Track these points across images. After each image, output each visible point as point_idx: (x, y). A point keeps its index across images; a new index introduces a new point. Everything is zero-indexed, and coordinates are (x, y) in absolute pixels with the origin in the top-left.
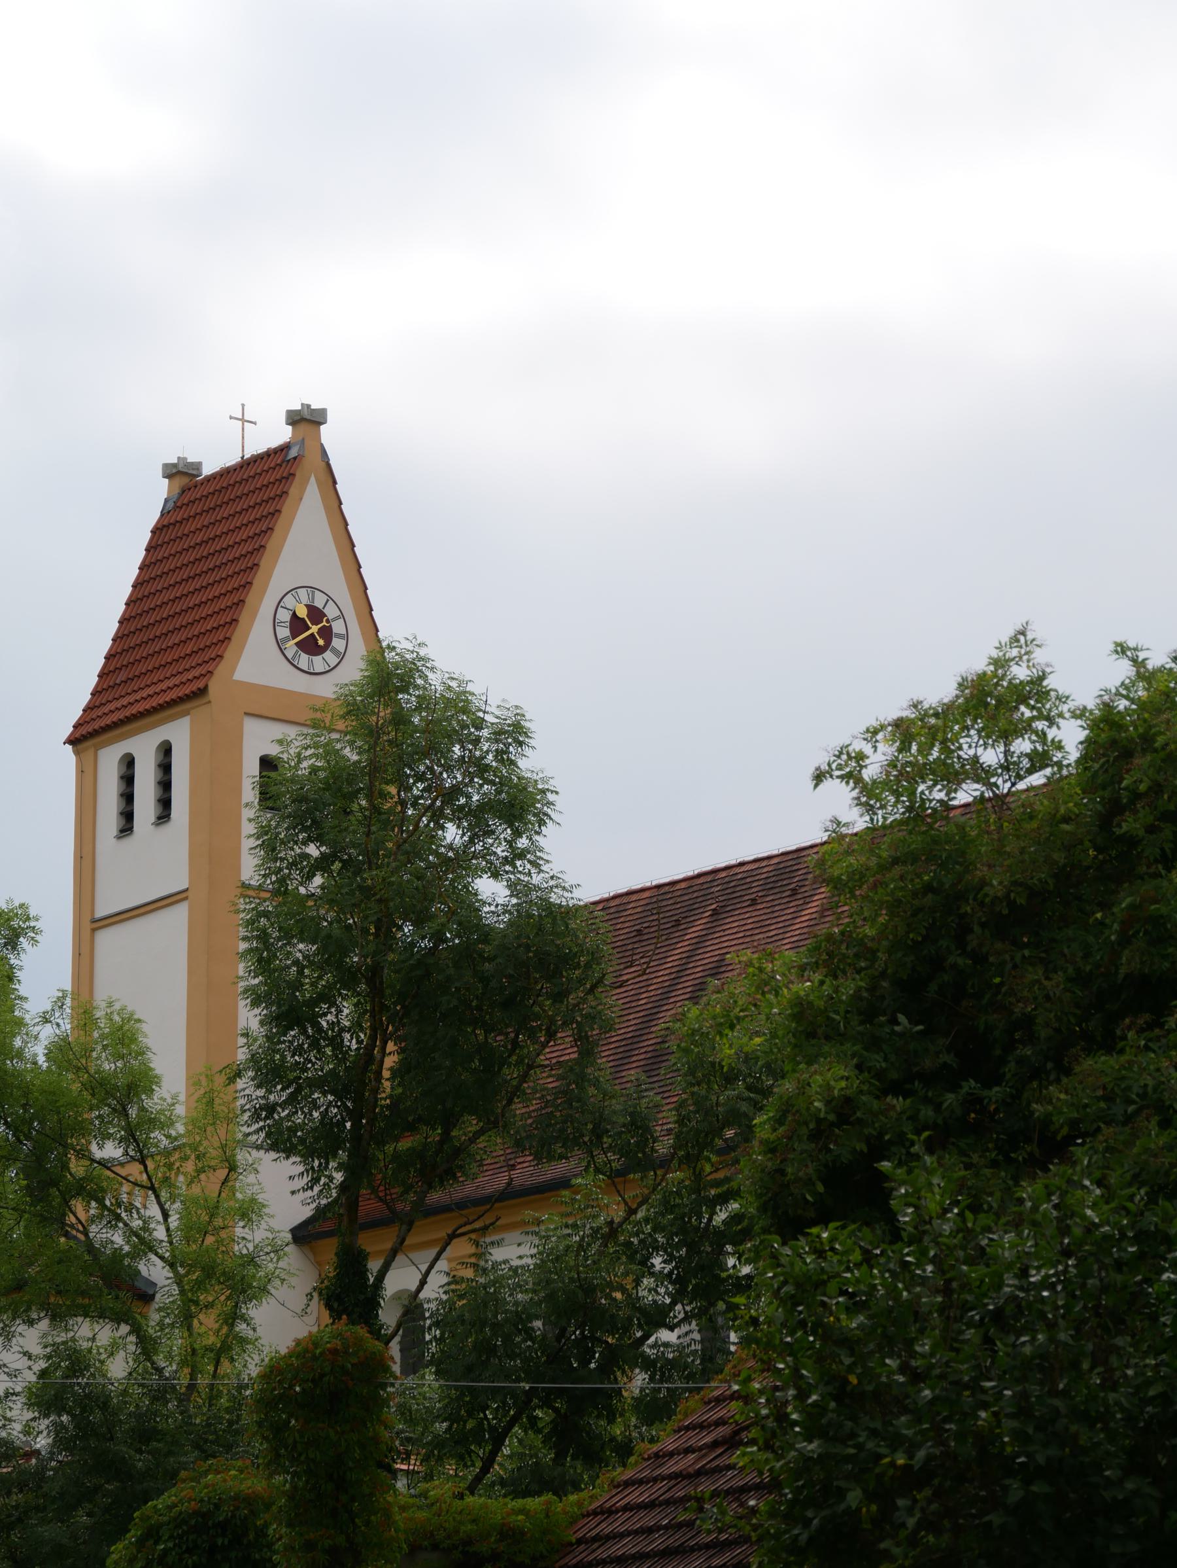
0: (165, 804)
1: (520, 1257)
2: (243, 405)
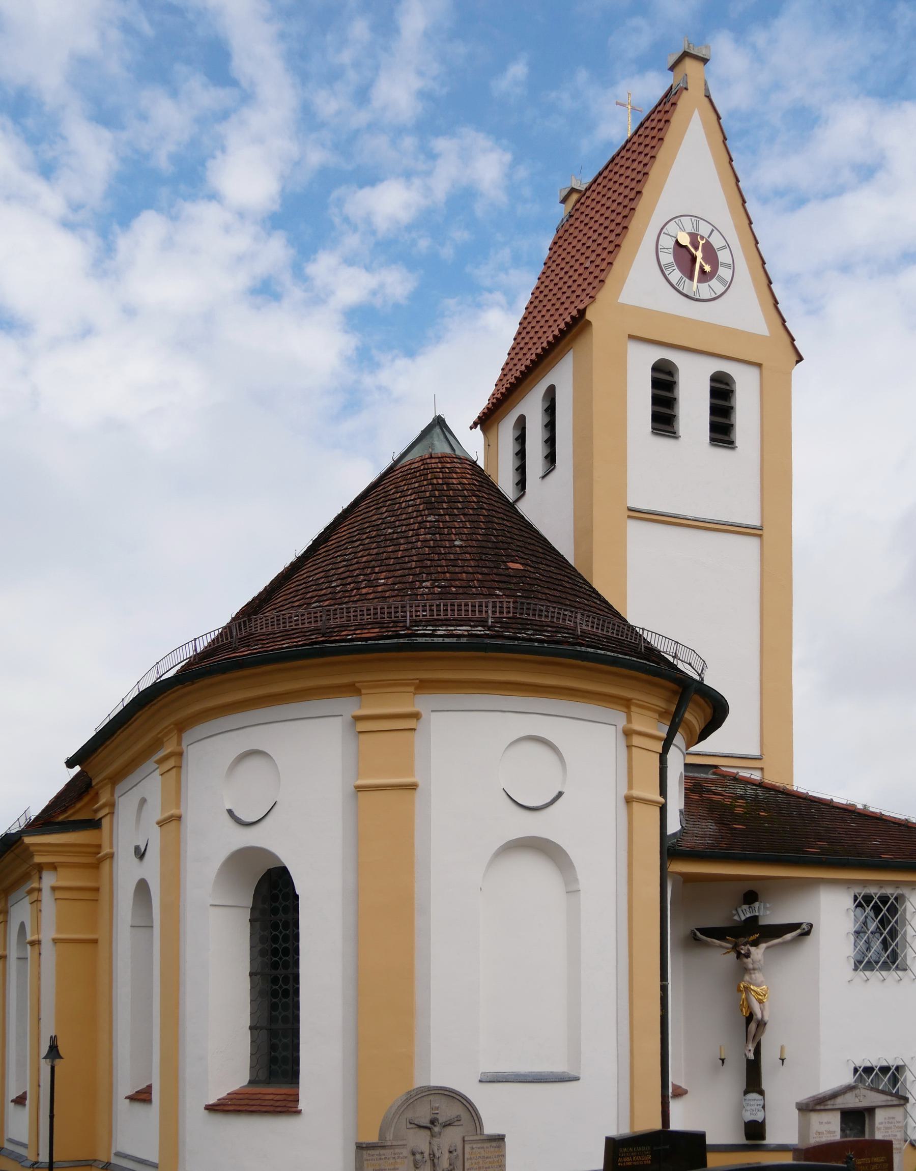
0: (551, 458)
1: (828, 1123)
2: (560, 794)
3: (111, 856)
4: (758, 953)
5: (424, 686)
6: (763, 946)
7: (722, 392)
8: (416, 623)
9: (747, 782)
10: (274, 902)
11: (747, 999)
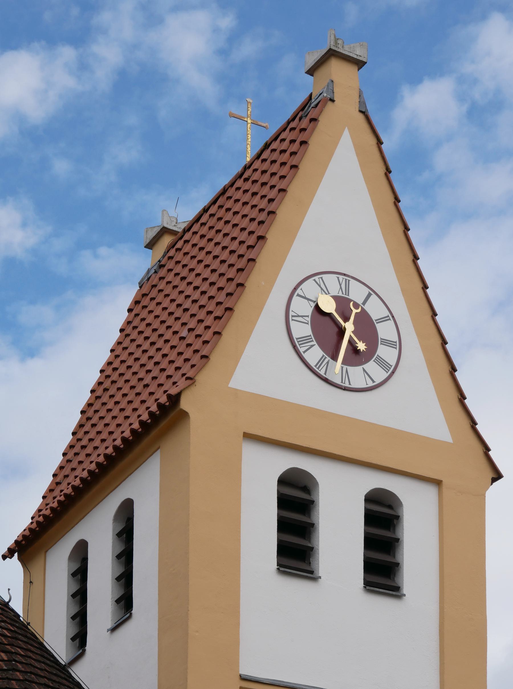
7: (382, 520)
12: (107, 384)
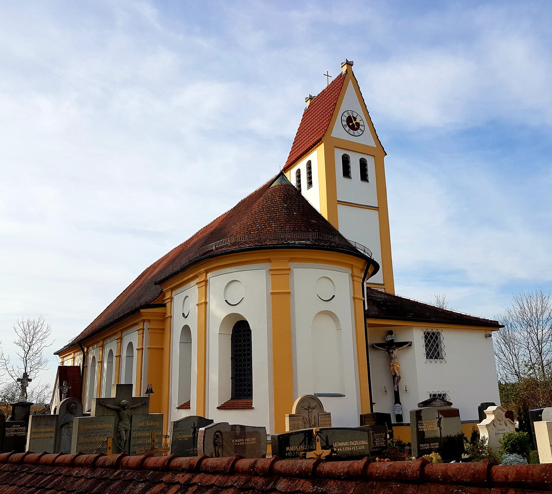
0: (310, 184)
2: (334, 296)
3: (171, 317)
4: (396, 352)
5: (292, 260)
6: (397, 350)
7: (363, 164)
8: (289, 239)
9: (381, 293)
10: (240, 333)
11: (393, 369)
12: (246, 363)
